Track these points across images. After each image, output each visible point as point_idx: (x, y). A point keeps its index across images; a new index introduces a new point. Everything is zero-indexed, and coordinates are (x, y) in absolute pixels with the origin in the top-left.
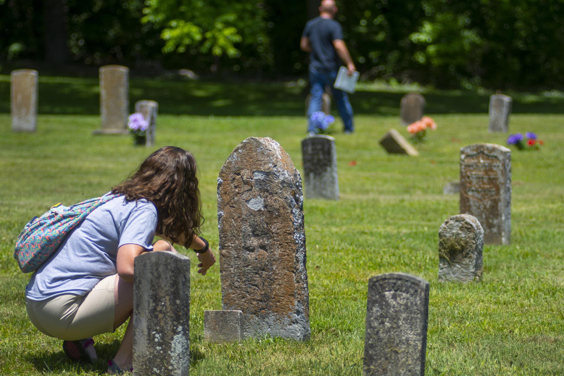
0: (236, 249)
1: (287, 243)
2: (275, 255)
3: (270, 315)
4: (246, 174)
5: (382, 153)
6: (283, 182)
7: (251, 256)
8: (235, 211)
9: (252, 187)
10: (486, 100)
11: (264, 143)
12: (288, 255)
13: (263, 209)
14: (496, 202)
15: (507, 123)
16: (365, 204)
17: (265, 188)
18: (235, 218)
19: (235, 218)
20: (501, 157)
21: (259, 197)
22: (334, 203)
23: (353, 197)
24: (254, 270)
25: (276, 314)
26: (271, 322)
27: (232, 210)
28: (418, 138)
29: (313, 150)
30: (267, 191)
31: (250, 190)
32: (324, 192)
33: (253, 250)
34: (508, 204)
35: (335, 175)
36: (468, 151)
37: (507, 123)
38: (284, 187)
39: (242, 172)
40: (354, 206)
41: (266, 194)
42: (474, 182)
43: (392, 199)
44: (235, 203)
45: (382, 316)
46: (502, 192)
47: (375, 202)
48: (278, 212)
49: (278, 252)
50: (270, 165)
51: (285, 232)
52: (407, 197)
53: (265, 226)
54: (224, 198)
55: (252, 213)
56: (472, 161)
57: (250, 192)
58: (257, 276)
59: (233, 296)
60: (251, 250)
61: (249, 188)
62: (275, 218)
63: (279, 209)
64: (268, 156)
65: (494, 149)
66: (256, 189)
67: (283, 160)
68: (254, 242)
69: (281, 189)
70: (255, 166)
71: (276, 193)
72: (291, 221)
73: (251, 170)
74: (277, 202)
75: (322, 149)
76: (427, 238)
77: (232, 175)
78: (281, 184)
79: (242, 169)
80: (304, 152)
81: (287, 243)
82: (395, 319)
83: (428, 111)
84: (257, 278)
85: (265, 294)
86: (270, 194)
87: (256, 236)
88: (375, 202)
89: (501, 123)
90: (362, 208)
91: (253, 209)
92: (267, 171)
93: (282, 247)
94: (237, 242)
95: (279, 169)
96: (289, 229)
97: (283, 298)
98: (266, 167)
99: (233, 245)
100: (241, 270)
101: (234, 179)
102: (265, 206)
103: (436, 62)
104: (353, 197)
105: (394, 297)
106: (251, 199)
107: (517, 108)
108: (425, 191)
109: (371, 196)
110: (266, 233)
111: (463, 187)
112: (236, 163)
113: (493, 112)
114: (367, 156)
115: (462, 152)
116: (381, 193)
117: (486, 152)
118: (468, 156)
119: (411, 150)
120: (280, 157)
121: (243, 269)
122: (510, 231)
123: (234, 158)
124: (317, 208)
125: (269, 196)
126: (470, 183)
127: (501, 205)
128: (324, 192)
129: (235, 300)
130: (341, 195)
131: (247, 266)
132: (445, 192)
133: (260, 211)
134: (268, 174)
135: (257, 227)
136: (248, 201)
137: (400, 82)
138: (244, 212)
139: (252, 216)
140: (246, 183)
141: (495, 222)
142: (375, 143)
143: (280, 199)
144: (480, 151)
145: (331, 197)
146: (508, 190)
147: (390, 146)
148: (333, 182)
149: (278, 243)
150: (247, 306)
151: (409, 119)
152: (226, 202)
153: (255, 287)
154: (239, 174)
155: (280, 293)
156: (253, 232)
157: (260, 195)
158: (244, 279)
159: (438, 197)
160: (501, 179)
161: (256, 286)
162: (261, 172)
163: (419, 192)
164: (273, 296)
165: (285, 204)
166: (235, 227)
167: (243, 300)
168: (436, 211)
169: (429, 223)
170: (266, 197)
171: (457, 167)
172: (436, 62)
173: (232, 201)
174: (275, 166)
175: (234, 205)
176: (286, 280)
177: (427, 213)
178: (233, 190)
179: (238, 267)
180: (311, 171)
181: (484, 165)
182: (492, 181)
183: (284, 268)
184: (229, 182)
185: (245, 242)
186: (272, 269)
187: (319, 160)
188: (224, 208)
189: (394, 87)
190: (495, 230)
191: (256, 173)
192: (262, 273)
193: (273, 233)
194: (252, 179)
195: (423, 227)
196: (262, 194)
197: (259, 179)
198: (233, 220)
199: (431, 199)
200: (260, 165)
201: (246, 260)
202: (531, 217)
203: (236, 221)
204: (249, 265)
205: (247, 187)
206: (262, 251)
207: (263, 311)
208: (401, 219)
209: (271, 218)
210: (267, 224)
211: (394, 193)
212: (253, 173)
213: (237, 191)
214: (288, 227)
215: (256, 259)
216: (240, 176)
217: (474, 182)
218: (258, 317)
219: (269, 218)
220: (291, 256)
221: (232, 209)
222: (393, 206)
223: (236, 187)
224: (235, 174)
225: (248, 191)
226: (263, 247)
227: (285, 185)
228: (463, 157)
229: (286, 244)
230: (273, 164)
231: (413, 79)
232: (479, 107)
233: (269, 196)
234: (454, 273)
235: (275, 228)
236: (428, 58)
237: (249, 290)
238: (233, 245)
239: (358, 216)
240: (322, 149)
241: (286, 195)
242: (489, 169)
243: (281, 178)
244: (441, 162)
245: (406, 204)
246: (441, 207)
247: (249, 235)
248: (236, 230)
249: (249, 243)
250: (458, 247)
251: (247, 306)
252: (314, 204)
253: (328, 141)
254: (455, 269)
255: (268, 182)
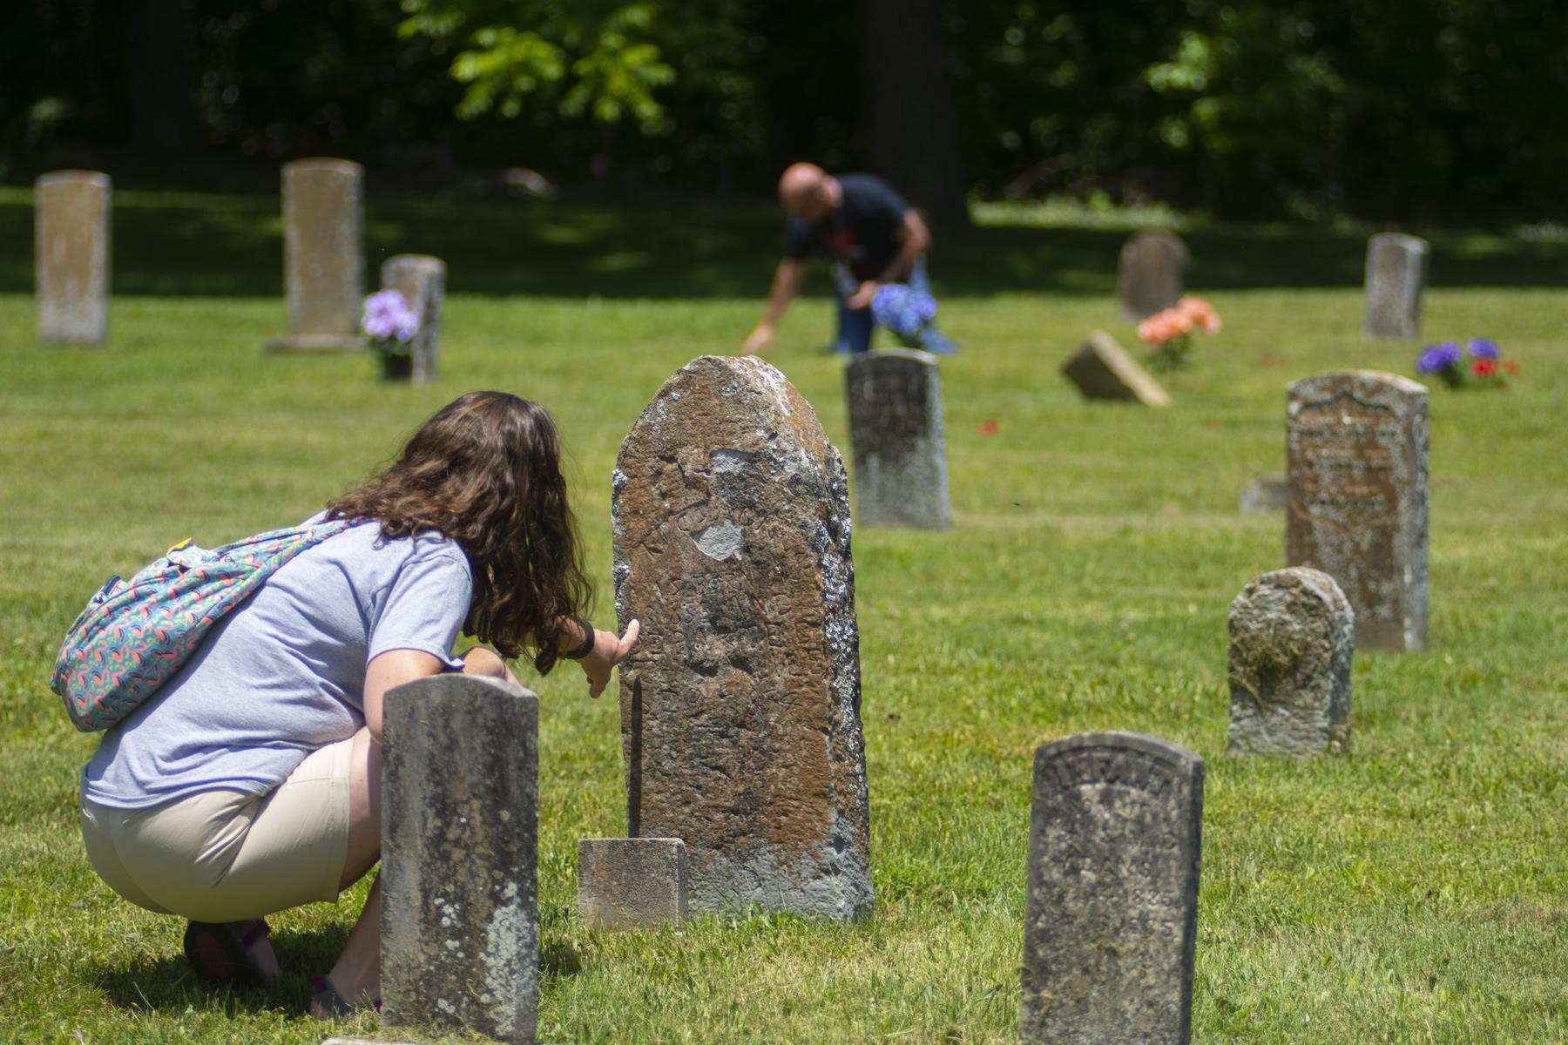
0: (665, 666)
1: (808, 650)
2: (773, 683)
3: (762, 850)
4: (691, 458)
5: (1069, 399)
6: (795, 481)
7: (707, 687)
8: (662, 563)
9: (709, 495)
10: (1359, 250)
11: (741, 372)
12: (810, 684)
13: (739, 557)
14: (1386, 535)
15: (1416, 312)
16: (1021, 541)
17: (745, 496)
18: (663, 581)
19: (663, 581)
20: (1400, 409)
21: (728, 523)
22: (936, 538)
23: (990, 522)
24: (716, 724)
25: (777, 847)
26: (764, 870)
27: (654, 560)
28: (1169, 356)
29: (876, 391)
30: (752, 506)
31: (705, 503)
32: (909, 509)
33: (711, 672)
34: (1421, 538)
35: (939, 461)
36: (1310, 393)
37: (1416, 312)
38: (798, 494)
39: (682, 453)
40: (993, 547)
41: (749, 514)
42: (1327, 477)
43: (1098, 527)
44: (663, 539)
45: (1072, 852)
46: (1403, 504)
47: (1052, 533)
48: (782, 565)
49: (781, 676)
50: (760, 433)
51: (800, 621)
52: (1138, 520)
53: (747, 602)
54: (632, 525)
55: (709, 568)
56: (1321, 420)
57: (704, 508)
58: (725, 741)
59: (659, 797)
60: (707, 669)
61: (701, 496)
62: (774, 580)
63: (783, 557)
64: (753, 408)
65: (1380, 387)
66: (719, 501)
67: (794, 419)
68: (716, 648)
69: (790, 501)
70: (717, 437)
71: (777, 512)
72: (819, 588)
73: (707, 447)
74: (777, 535)
75: (903, 389)
76: (1194, 634)
77: (652, 462)
78: (789, 486)
79: (682, 445)
80: (853, 398)
81: (808, 650)
82: (1108, 859)
83: (1198, 280)
84: (724, 748)
85: (748, 792)
86: (761, 513)
87: (723, 630)
88: (1052, 533)
89: (1400, 313)
90: (1015, 552)
91: (713, 555)
92: (749, 450)
93: (793, 662)
94: (668, 648)
95: (785, 445)
96: (811, 611)
97: (796, 803)
98: (749, 438)
99: (656, 657)
100: (680, 726)
101: (659, 473)
102: (747, 549)
103: (1218, 144)
104: (990, 522)
105: (1106, 799)
106: (705, 528)
107: (1444, 272)
108: (1190, 504)
109: (1040, 518)
110: (750, 623)
111: (1294, 492)
112: (665, 427)
113: (1377, 283)
114: (1027, 406)
115: (1293, 396)
116: (1067, 509)
117: (1358, 394)
118: (1308, 406)
119: (1150, 390)
120: (785, 411)
121: (685, 722)
122: (1425, 615)
123: (659, 415)
124: (889, 553)
125: (757, 521)
126: (1315, 480)
127: (1401, 542)
128: (909, 509)
129: (663, 811)
130: (956, 516)
131: (696, 716)
132: (1246, 506)
133: (731, 560)
134: (752, 458)
135: (724, 608)
136: (697, 534)
137: (1117, 200)
138: (688, 565)
139: (708, 576)
140: (693, 484)
141: (1386, 588)
142: (1048, 371)
143: (786, 529)
144: (1343, 393)
145: (929, 522)
146: (1420, 500)
147: (1092, 378)
148: (933, 480)
149: (783, 649)
150: (697, 825)
151: (1144, 304)
152: (638, 536)
153: (718, 773)
154: (671, 460)
155: (788, 789)
156: (713, 620)
157: (730, 517)
158: (688, 751)
159: (1226, 522)
160: (1401, 470)
161: (722, 769)
162: (734, 453)
163: (1173, 508)
164: (769, 799)
165: (802, 542)
166: (661, 606)
167: (687, 810)
168: (1219, 559)
169: (1200, 594)
170: (749, 522)
171: (1278, 437)
172: (1218, 144)
173: (655, 534)
174: (773, 436)
175: (660, 546)
176: (804, 753)
177: (1194, 566)
178: (656, 503)
179: (671, 718)
180: (872, 448)
181: (1353, 431)
182: (1376, 475)
183: (799, 721)
184: (645, 481)
185: (691, 648)
186: (766, 724)
187: (894, 419)
188: (630, 553)
189: (1101, 214)
190: (1384, 611)
191: (721, 457)
192: (737, 734)
193: (767, 623)
194: (708, 472)
195: (1184, 603)
196: (736, 514)
197: (729, 473)
198: (655, 587)
199: (1207, 526)
200: (732, 433)
201: (693, 697)
202: (1485, 576)
203: (664, 589)
204: (702, 712)
205: (695, 496)
206: (737, 673)
207: (742, 839)
208: (1124, 582)
209: (762, 580)
210: (752, 597)
211: (1101, 509)
212: (712, 455)
213: (667, 505)
214: (810, 605)
215: (722, 696)
216: (675, 465)
217: (1327, 477)
218: (727, 855)
219: (758, 580)
220: (818, 688)
221: (654, 557)
222: (1102, 547)
223: (664, 496)
224: (662, 458)
225: (697, 505)
226: (740, 662)
227: (800, 488)
228: (1294, 407)
229: (804, 654)
230: (767, 430)
231: (1157, 193)
232: (1338, 269)
233: (757, 521)
234: (1271, 732)
235: (772, 608)
236: (1196, 133)
237: (702, 780)
238: (656, 657)
239: (1004, 575)
240: (903, 389)
241: (802, 517)
242: (1366, 443)
243: (791, 469)
244: (1233, 424)
245: (1137, 539)
246: (1235, 548)
247: (701, 629)
248: (666, 615)
249: (700, 650)
250: (1283, 660)
251: (697, 825)
252: (880, 542)
253: (920, 367)
254: (1274, 719)
255: (752, 480)
